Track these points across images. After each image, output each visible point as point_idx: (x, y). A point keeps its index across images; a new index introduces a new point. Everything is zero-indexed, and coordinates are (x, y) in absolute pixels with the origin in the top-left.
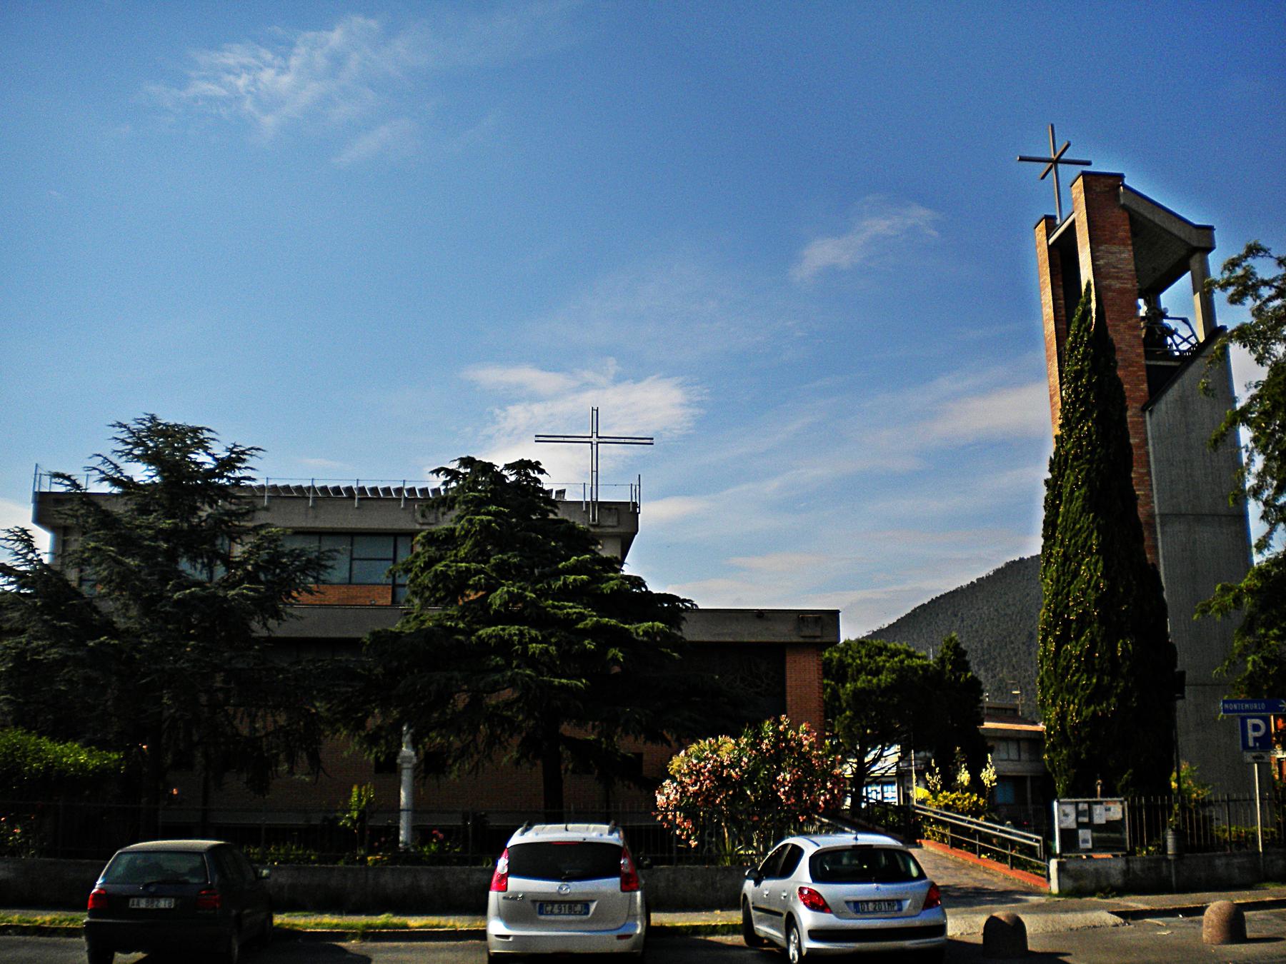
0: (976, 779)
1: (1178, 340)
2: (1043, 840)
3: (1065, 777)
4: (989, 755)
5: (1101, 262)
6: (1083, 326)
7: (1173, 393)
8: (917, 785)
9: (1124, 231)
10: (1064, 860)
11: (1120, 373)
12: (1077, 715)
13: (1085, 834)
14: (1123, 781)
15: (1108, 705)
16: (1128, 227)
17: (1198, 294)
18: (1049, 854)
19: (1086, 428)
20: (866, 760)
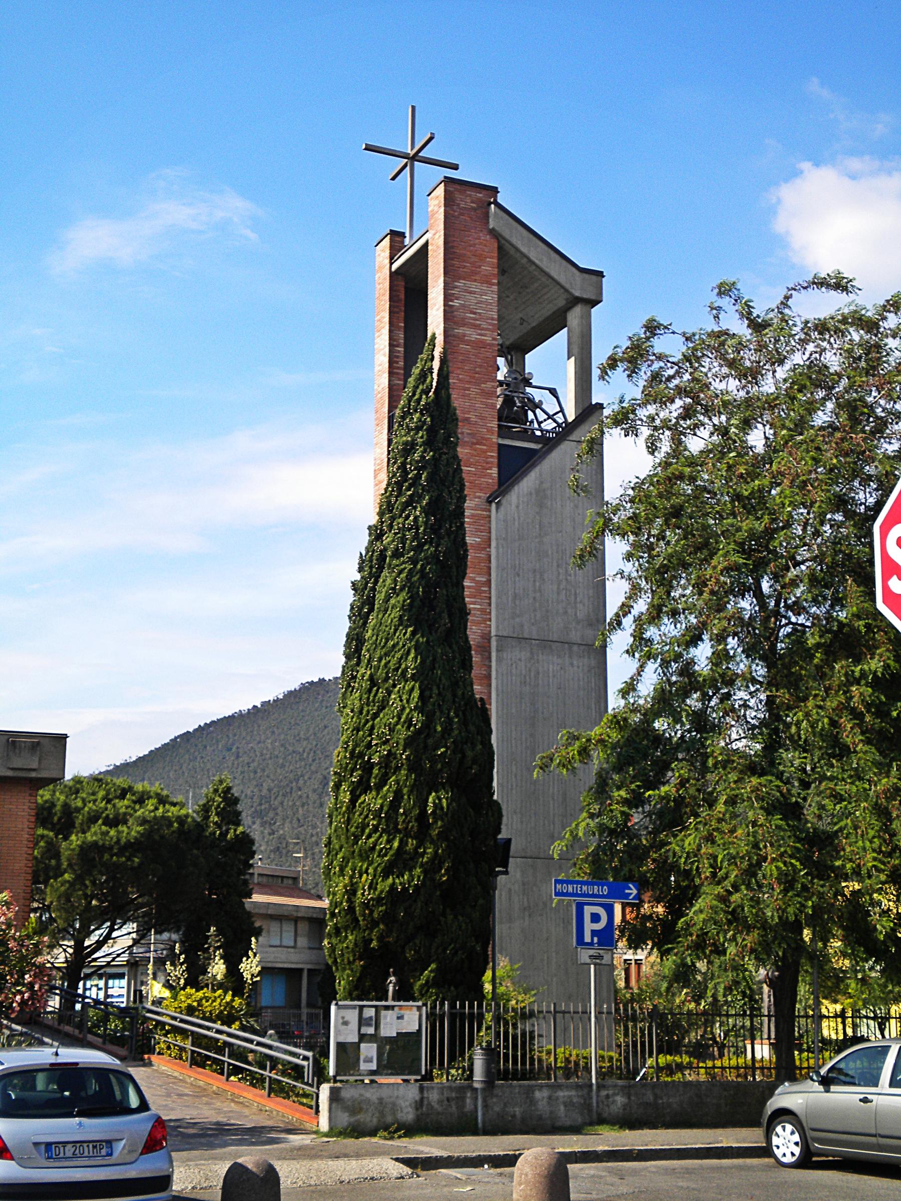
0: (233, 971)
1: (542, 416)
2: (314, 1056)
3: (348, 972)
4: (253, 939)
5: (456, 303)
6: (421, 387)
7: (528, 483)
8: (155, 978)
9: (490, 266)
10: (338, 1085)
11: (462, 451)
12: (370, 888)
13: (369, 1050)
14: (422, 981)
15: (412, 877)
16: (495, 261)
17: (573, 359)
18: (320, 1074)
19: (411, 518)
20: (87, 943)
